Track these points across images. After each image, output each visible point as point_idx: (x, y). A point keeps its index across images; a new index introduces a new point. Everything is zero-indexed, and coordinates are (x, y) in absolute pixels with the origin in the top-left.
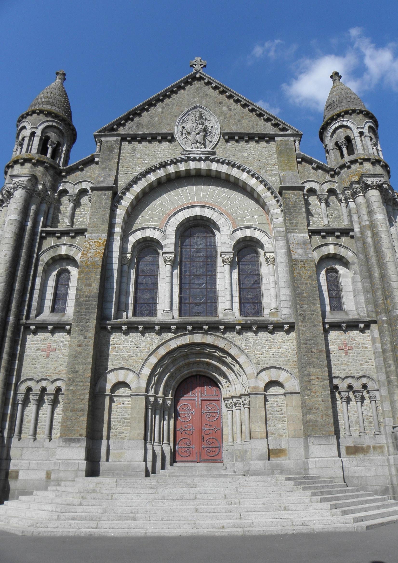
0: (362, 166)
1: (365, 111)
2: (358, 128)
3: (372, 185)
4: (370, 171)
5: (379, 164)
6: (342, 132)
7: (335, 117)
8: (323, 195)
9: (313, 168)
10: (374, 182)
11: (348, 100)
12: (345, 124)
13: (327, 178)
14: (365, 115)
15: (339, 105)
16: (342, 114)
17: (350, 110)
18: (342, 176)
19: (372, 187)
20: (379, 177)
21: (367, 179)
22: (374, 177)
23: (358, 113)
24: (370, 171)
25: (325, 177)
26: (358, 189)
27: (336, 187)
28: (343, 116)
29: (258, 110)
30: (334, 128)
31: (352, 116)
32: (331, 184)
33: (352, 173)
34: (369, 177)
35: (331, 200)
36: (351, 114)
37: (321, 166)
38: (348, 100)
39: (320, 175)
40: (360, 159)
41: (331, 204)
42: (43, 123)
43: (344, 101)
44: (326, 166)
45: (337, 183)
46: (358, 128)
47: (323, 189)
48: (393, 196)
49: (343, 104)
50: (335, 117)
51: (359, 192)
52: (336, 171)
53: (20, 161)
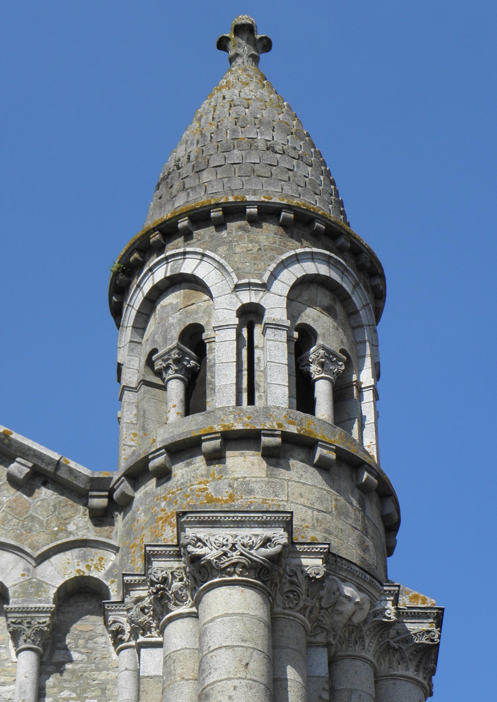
0: (215, 468)
1: (289, 208)
2: (237, 287)
3: (225, 562)
4: (250, 492)
5: (309, 461)
6: (175, 308)
7: (156, 237)
8: (27, 611)
9: (12, 480)
10: (233, 548)
11: (236, 155)
12: (189, 272)
13: (71, 527)
14: (286, 226)
15: (189, 183)
16: (183, 223)
17: (217, 205)
18: (134, 519)
19: (223, 571)
20: (264, 524)
21: (202, 533)
22: (240, 524)
23: (255, 221)
24: (250, 492)
25: (65, 521)
26: (177, 584)
27: (109, 574)
28: (188, 235)
29: (365, 251)
30: (147, 287)
31: (224, 234)
32: (84, 558)
33: (170, 504)
34: (214, 523)
35: (77, 638)
36: (220, 225)
37: (50, 469)
38: (236, 155)
39: (41, 515)
40: (211, 435)
41: (75, 656)
42: (284, 264)
43: (216, 160)
44: (71, 471)
45: (116, 549)
46: (237, 287)
47: (40, 586)
48: (375, 614)
49: (206, 176)
50: (156, 237)
51: (179, 600)
52: (115, 495)
53: (152, 464)
